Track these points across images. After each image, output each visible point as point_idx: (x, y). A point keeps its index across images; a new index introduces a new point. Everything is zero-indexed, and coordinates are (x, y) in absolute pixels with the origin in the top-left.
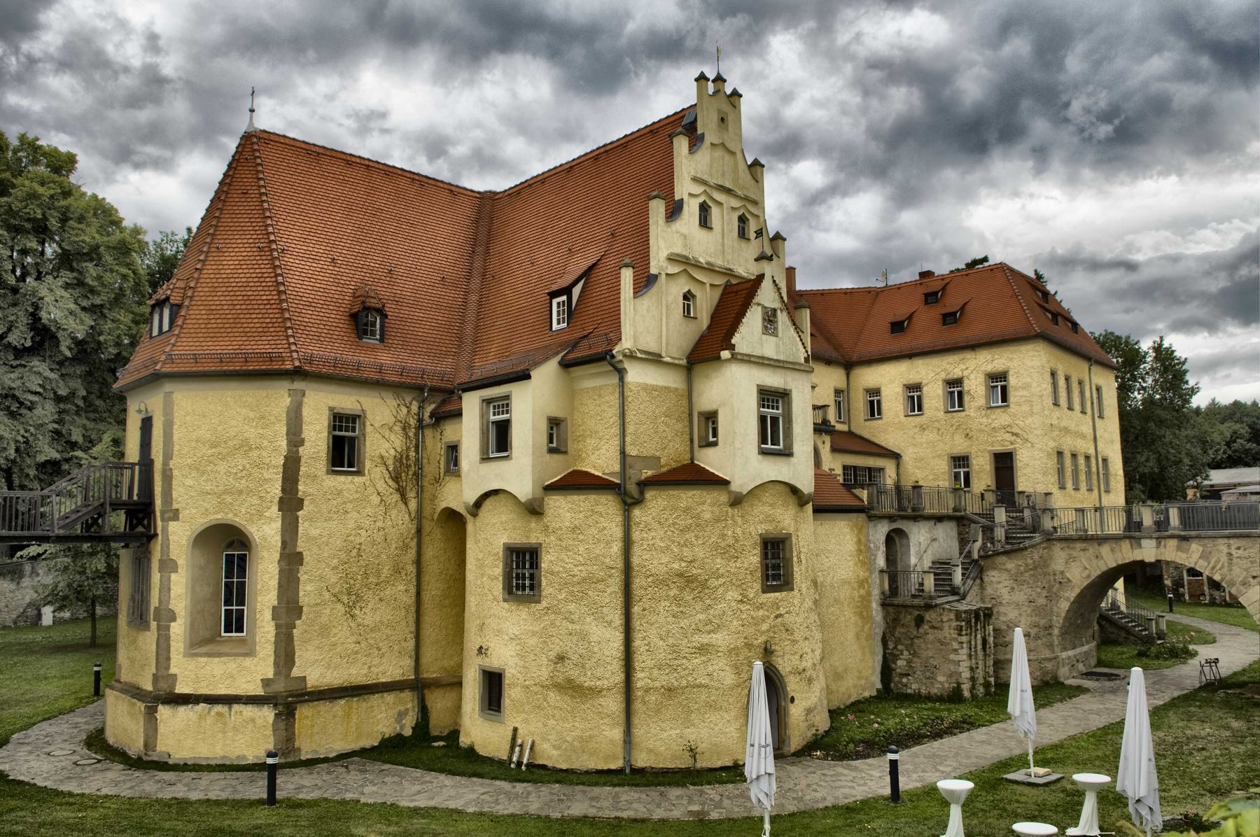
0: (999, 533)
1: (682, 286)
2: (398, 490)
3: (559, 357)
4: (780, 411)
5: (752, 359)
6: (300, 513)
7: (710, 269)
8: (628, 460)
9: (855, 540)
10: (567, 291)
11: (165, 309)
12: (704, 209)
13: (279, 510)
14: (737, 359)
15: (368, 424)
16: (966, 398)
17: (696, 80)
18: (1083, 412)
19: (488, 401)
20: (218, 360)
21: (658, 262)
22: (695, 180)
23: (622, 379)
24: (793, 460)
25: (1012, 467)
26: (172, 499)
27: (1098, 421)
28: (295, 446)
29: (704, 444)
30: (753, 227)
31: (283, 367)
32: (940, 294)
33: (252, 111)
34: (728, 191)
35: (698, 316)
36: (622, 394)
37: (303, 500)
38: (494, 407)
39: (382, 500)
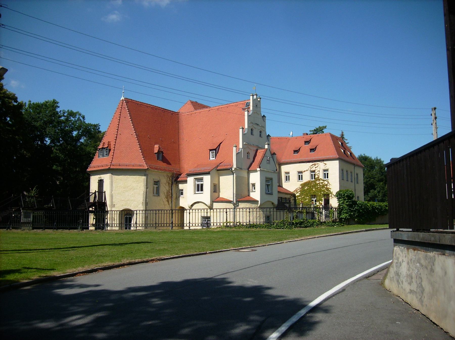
2: (167, 201)
18: (352, 182)
19: (195, 179)
27: (356, 185)
30: (263, 134)
35: (250, 158)
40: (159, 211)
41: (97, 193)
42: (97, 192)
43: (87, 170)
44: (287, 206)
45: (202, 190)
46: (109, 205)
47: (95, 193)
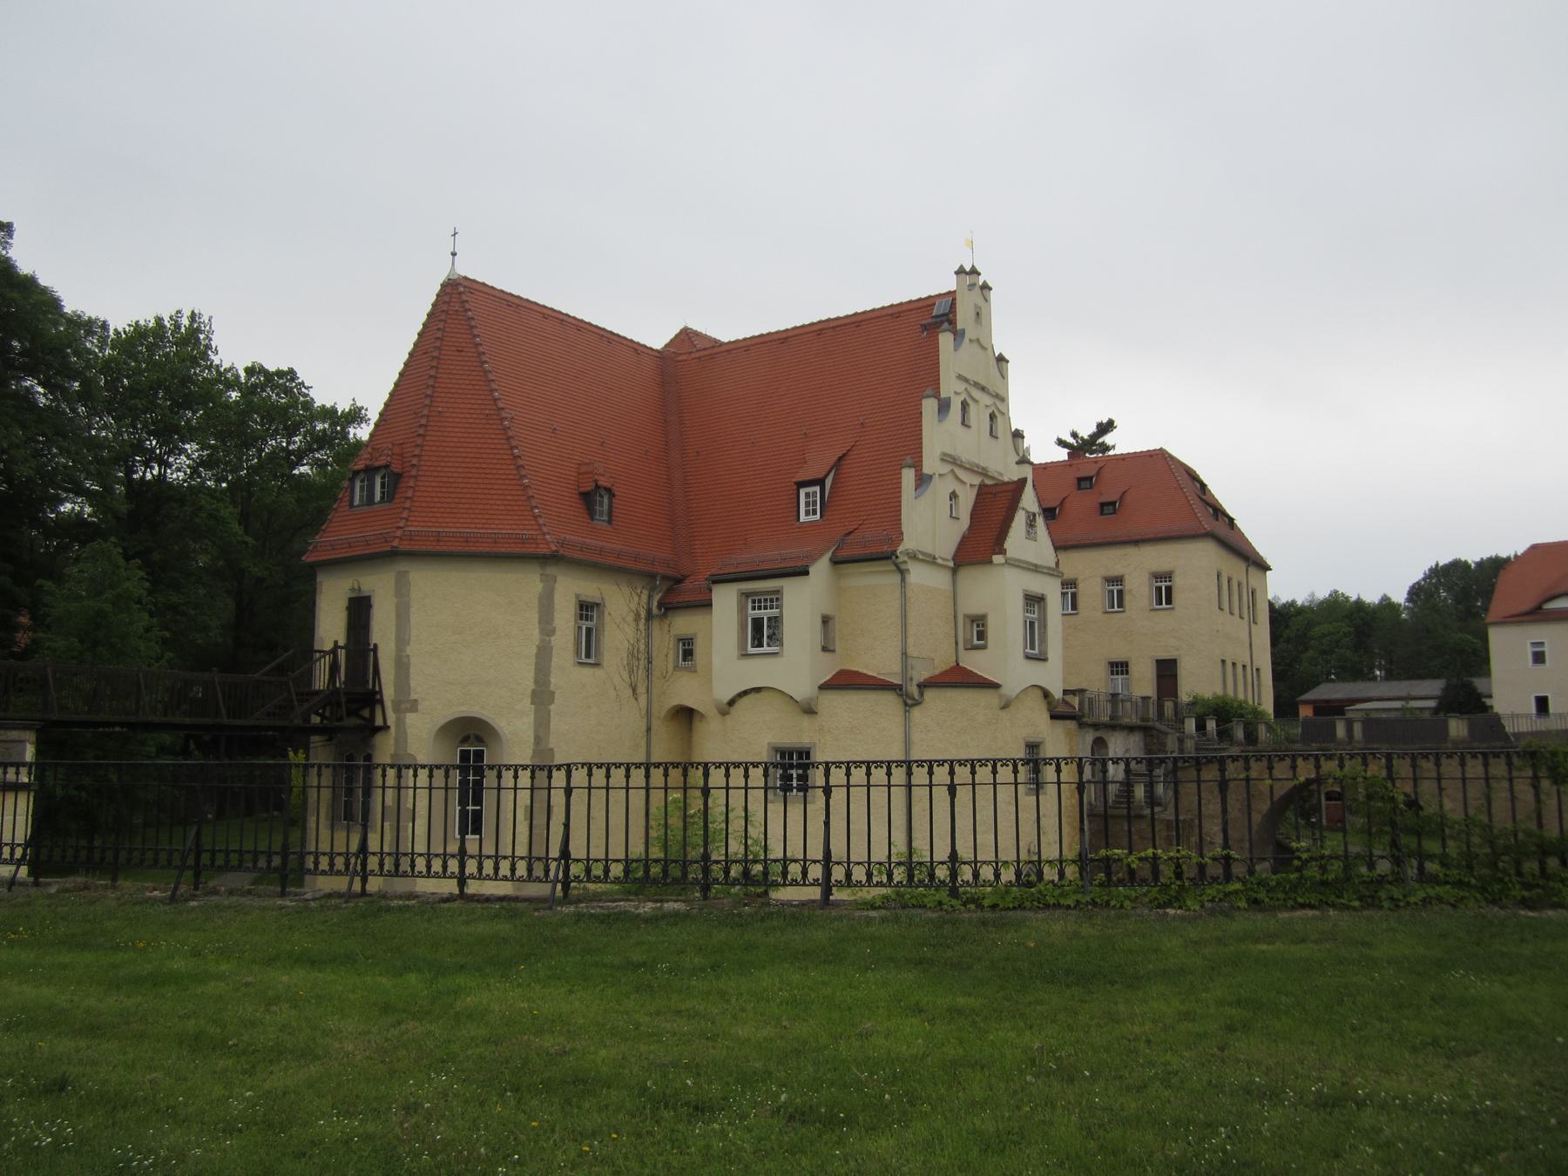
0: (1189, 745)
1: (950, 485)
3: (828, 555)
4: (1036, 616)
5: (1021, 565)
6: (552, 707)
7: (973, 469)
8: (910, 661)
9: (1068, 747)
10: (820, 482)
11: (376, 477)
12: (964, 405)
13: (532, 704)
14: (1009, 564)
15: (606, 613)
16: (1127, 598)
17: (957, 273)
19: (747, 595)
20: (383, 540)
21: (930, 464)
22: (961, 378)
23: (903, 580)
24: (1048, 664)
25: (1175, 676)
26: (409, 688)
28: (548, 636)
29: (970, 647)
31: (538, 550)
32: (1094, 479)
33: (454, 254)
34: (983, 389)
35: (960, 516)
36: (904, 594)
37: (554, 693)
38: (754, 602)
39: (617, 695)
40: (727, 775)
41: (343, 651)
42: (341, 648)
43: (303, 558)
44: (1072, 703)
45: (775, 638)
46: (393, 701)
47: (334, 651)
